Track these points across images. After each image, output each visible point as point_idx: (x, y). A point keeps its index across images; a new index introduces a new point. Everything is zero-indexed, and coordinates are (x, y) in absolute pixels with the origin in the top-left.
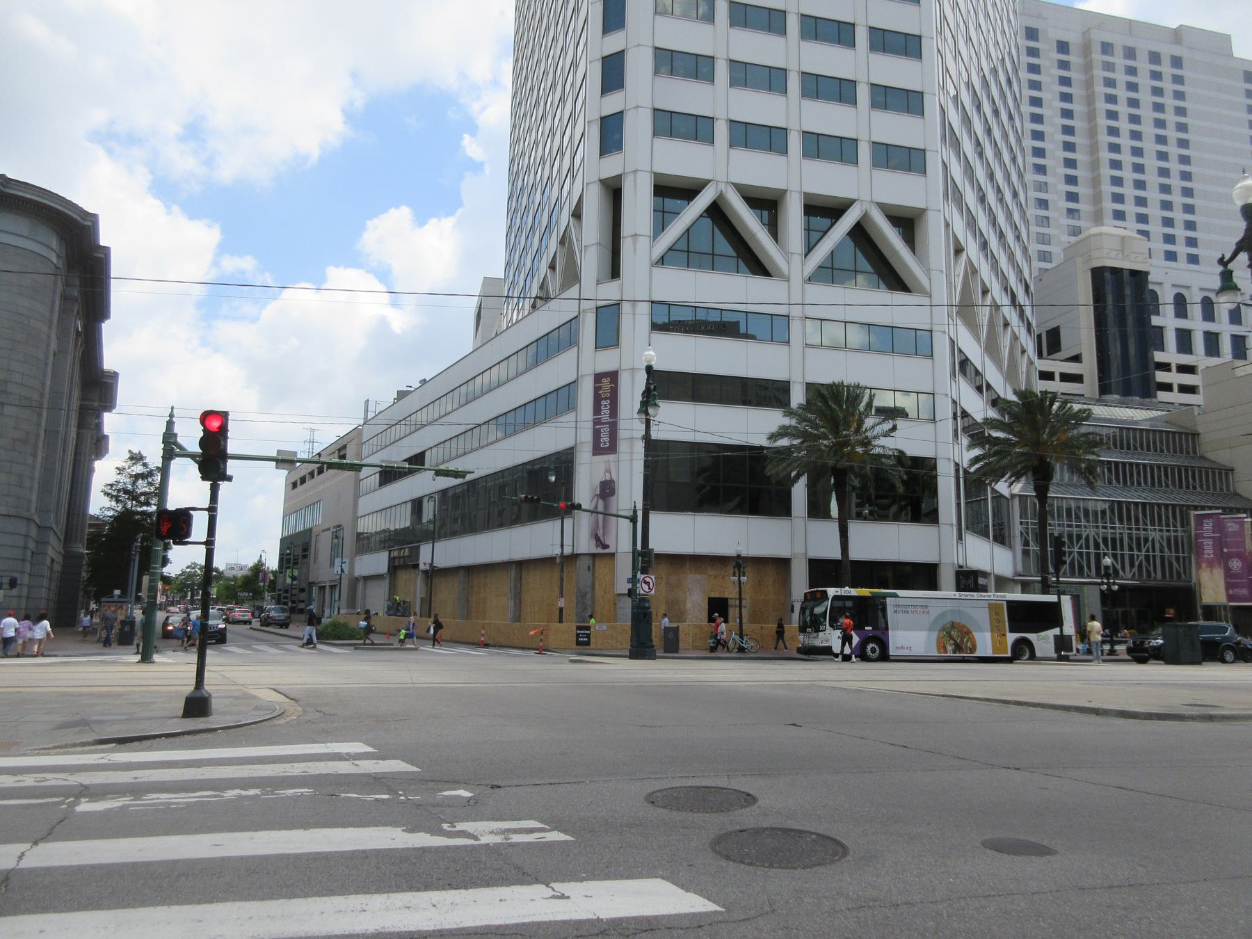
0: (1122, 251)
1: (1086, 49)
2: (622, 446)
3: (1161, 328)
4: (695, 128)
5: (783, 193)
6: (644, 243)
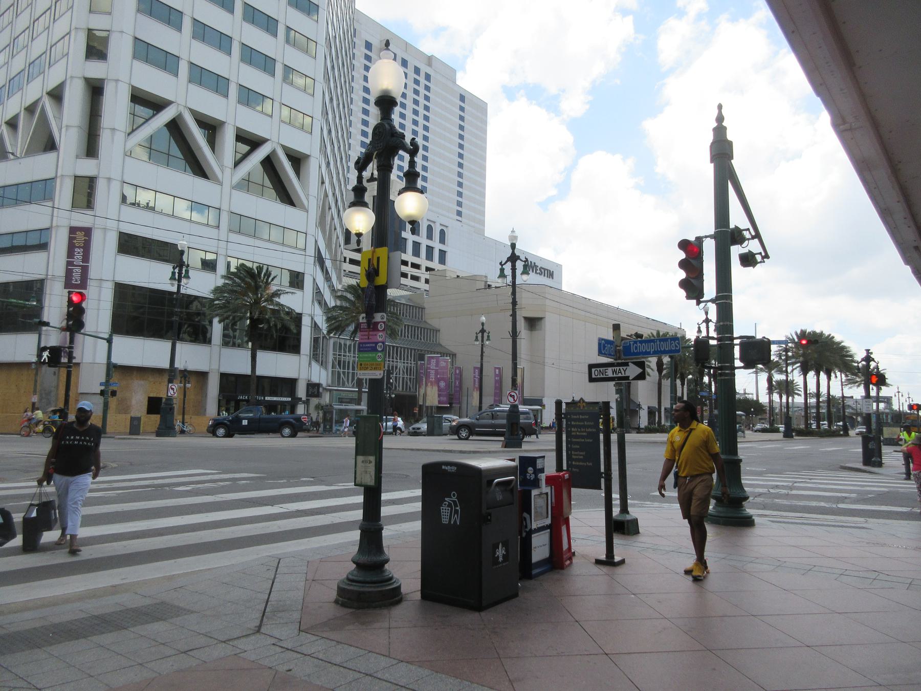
3: (406, 239)
4: (166, 61)
5: (222, 123)
6: (120, 137)
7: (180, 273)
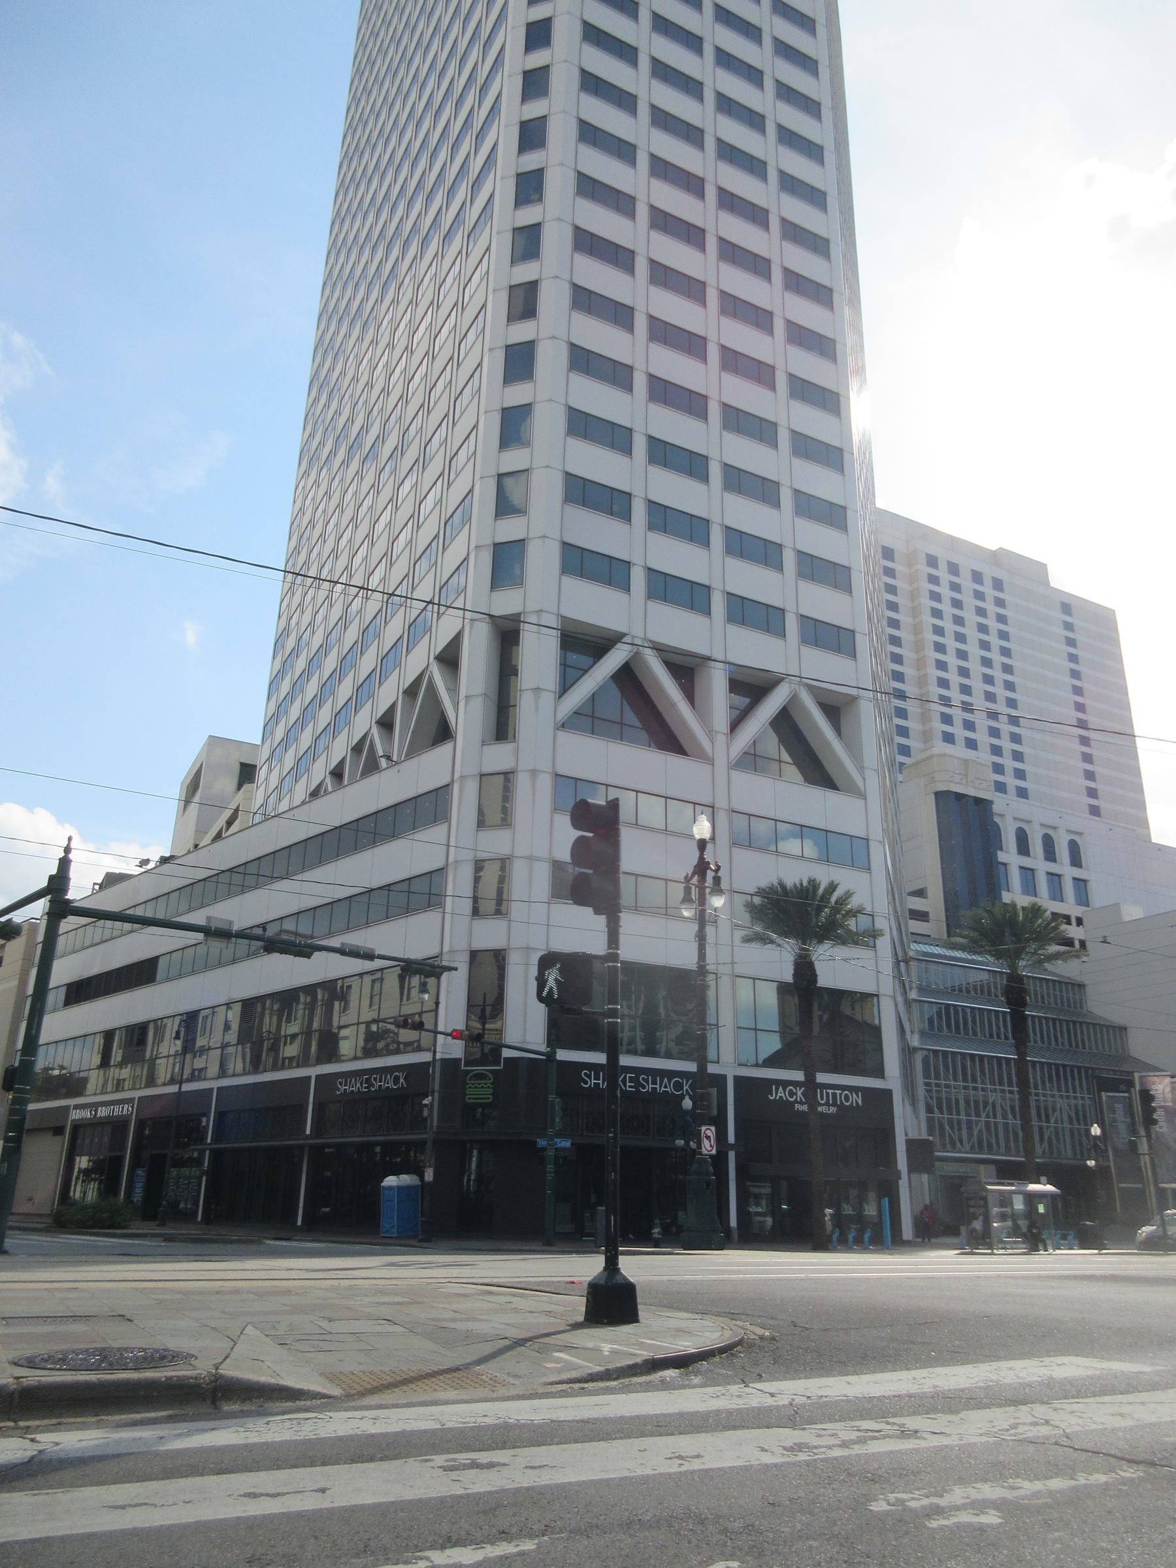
0: (966, 775)
4: (610, 571)
6: (548, 699)
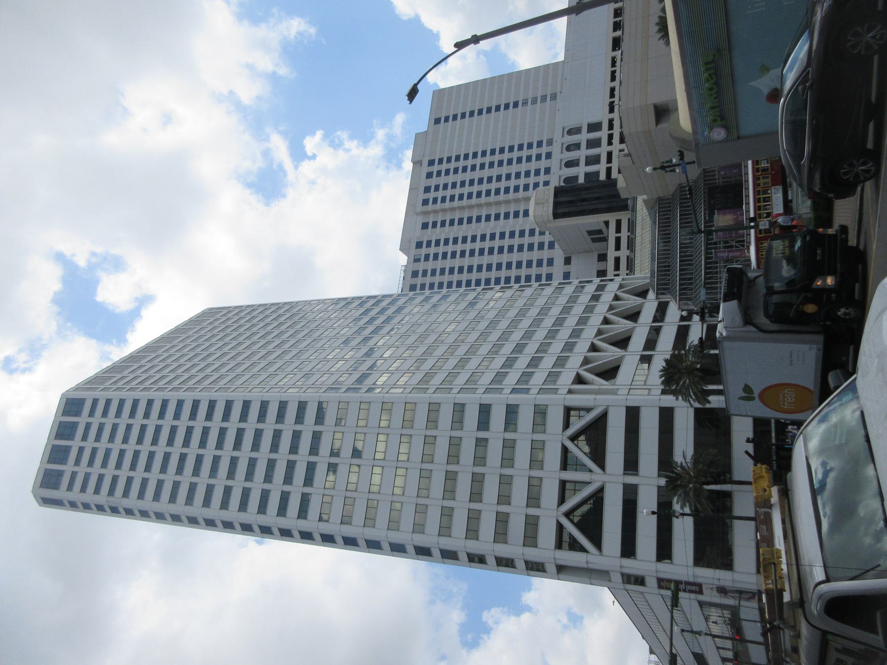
1: (427, 213)
2: (699, 580)
6: (590, 558)
7: (669, 166)
